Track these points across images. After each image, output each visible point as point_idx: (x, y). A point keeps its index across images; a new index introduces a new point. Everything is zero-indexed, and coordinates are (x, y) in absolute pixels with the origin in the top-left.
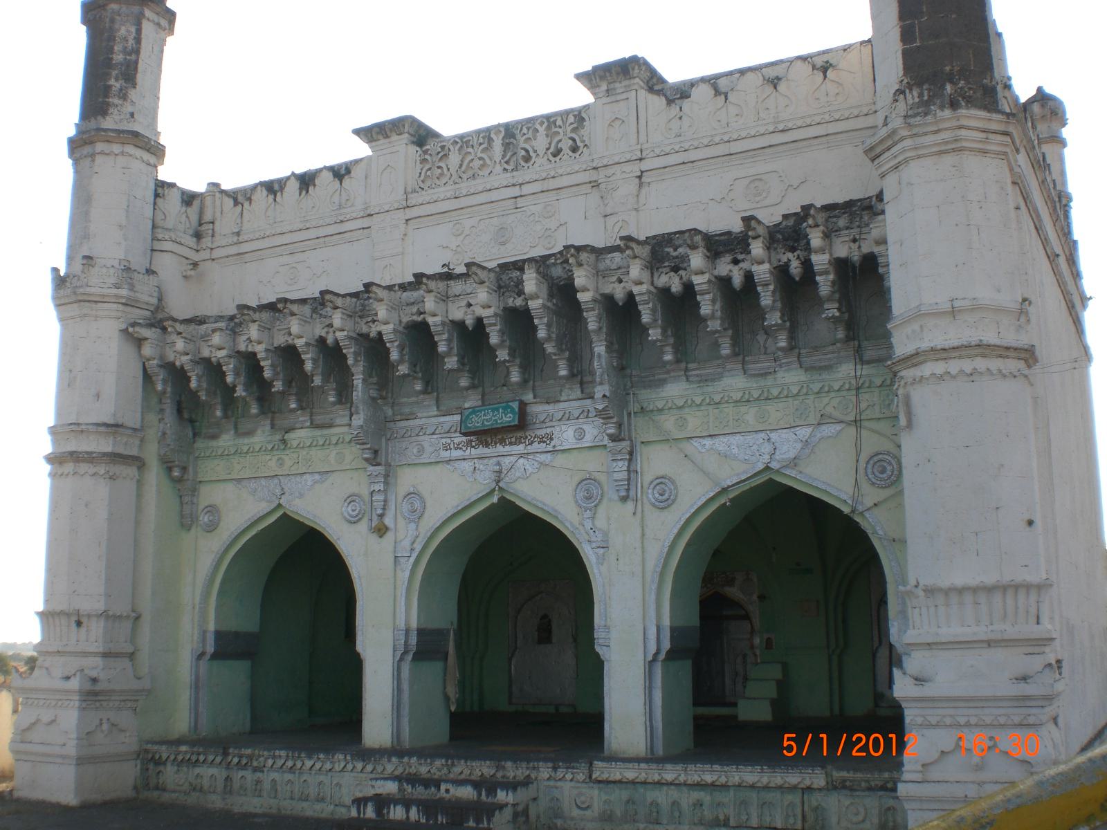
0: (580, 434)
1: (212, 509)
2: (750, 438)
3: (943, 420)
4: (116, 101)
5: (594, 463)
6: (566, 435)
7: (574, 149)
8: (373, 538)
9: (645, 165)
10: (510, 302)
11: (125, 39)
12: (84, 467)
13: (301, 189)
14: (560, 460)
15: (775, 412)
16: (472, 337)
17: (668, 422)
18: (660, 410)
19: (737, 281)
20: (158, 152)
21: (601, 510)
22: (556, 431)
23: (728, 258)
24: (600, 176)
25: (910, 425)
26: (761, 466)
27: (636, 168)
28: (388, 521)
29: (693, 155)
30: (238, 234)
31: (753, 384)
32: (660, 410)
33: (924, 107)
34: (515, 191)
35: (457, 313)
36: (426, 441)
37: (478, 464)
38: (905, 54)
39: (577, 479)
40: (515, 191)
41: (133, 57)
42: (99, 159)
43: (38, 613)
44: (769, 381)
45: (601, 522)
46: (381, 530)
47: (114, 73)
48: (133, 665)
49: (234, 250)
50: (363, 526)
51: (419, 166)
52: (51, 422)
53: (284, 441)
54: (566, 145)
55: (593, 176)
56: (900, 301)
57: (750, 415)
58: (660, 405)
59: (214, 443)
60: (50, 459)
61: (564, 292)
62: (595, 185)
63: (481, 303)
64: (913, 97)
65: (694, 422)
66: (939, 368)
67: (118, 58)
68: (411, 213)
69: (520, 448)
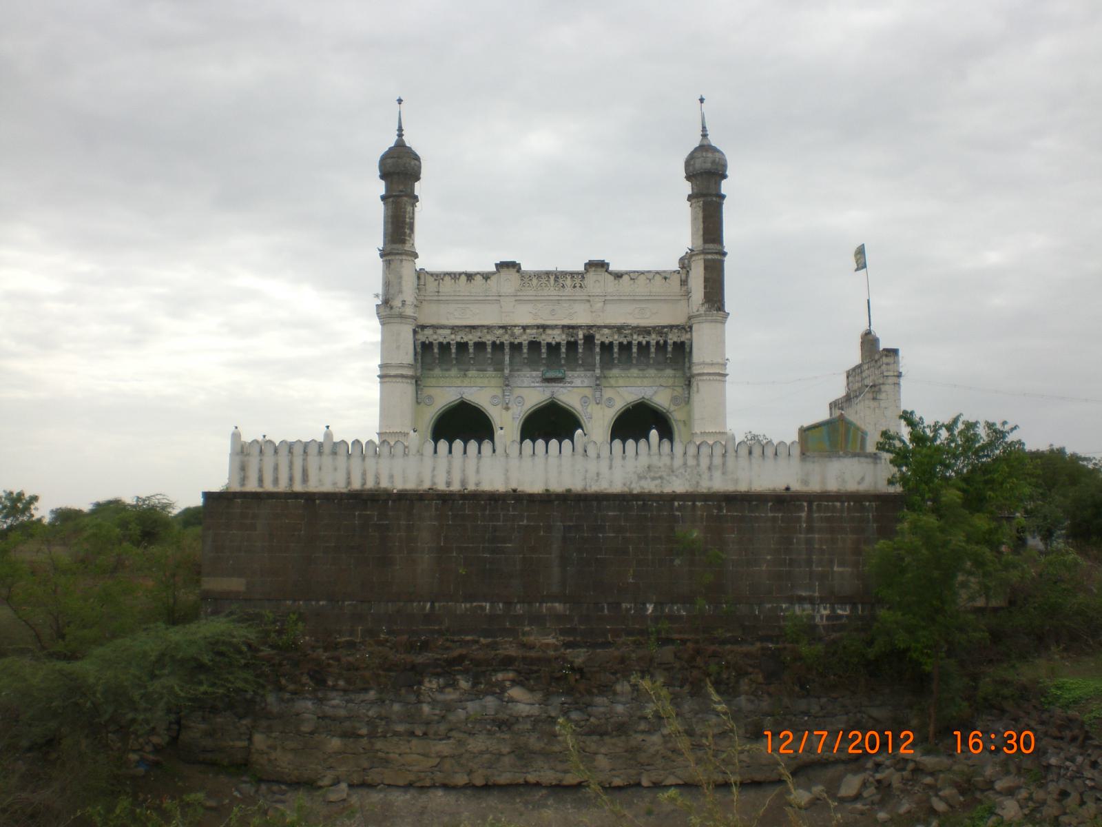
0: (582, 382)
1: (430, 397)
2: (638, 389)
3: (703, 392)
4: (408, 238)
5: (588, 392)
6: (578, 382)
7: (581, 287)
8: (504, 411)
9: (607, 298)
10: (569, 339)
11: (409, 213)
12: (404, 380)
13: (468, 280)
14: (575, 389)
15: (646, 382)
16: (553, 348)
17: (613, 382)
18: (610, 377)
19: (644, 343)
20: (416, 256)
21: (590, 407)
22: (574, 380)
23: (642, 336)
24: (591, 299)
25: (698, 391)
26: (641, 397)
27: (603, 299)
28: (509, 405)
29: (622, 298)
30: (438, 292)
31: (640, 372)
32: (610, 377)
33: (709, 309)
34: (559, 298)
35: (550, 340)
36: (525, 379)
37: (545, 389)
38: (705, 292)
39: (580, 397)
40: (559, 298)
41: (412, 221)
42: (404, 262)
43: (377, 434)
44: (645, 372)
45: (589, 410)
46: (507, 409)
47: (407, 226)
48: (261, 460)
49: (435, 298)
50: (499, 406)
51: (520, 282)
52: (1069, 451)
53: (465, 374)
54: (578, 285)
55: (588, 298)
56: (696, 357)
57: (639, 382)
58: (611, 376)
59: (432, 372)
60: (379, 376)
61: (589, 339)
62: (589, 301)
63: (558, 337)
64: (706, 306)
65: (621, 382)
66: (708, 378)
67: (408, 220)
68: (517, 298)
69: (562, 385)
